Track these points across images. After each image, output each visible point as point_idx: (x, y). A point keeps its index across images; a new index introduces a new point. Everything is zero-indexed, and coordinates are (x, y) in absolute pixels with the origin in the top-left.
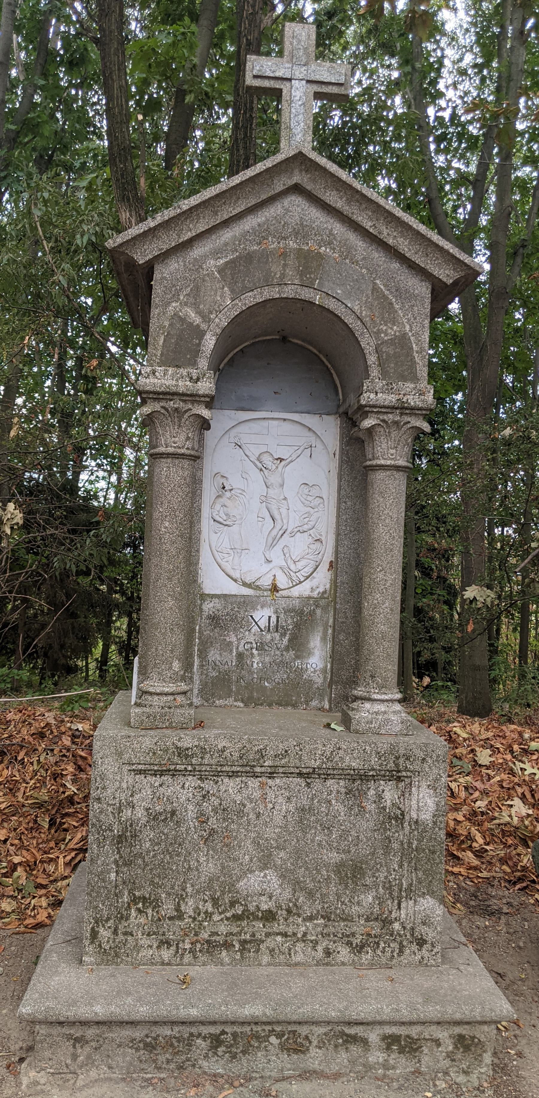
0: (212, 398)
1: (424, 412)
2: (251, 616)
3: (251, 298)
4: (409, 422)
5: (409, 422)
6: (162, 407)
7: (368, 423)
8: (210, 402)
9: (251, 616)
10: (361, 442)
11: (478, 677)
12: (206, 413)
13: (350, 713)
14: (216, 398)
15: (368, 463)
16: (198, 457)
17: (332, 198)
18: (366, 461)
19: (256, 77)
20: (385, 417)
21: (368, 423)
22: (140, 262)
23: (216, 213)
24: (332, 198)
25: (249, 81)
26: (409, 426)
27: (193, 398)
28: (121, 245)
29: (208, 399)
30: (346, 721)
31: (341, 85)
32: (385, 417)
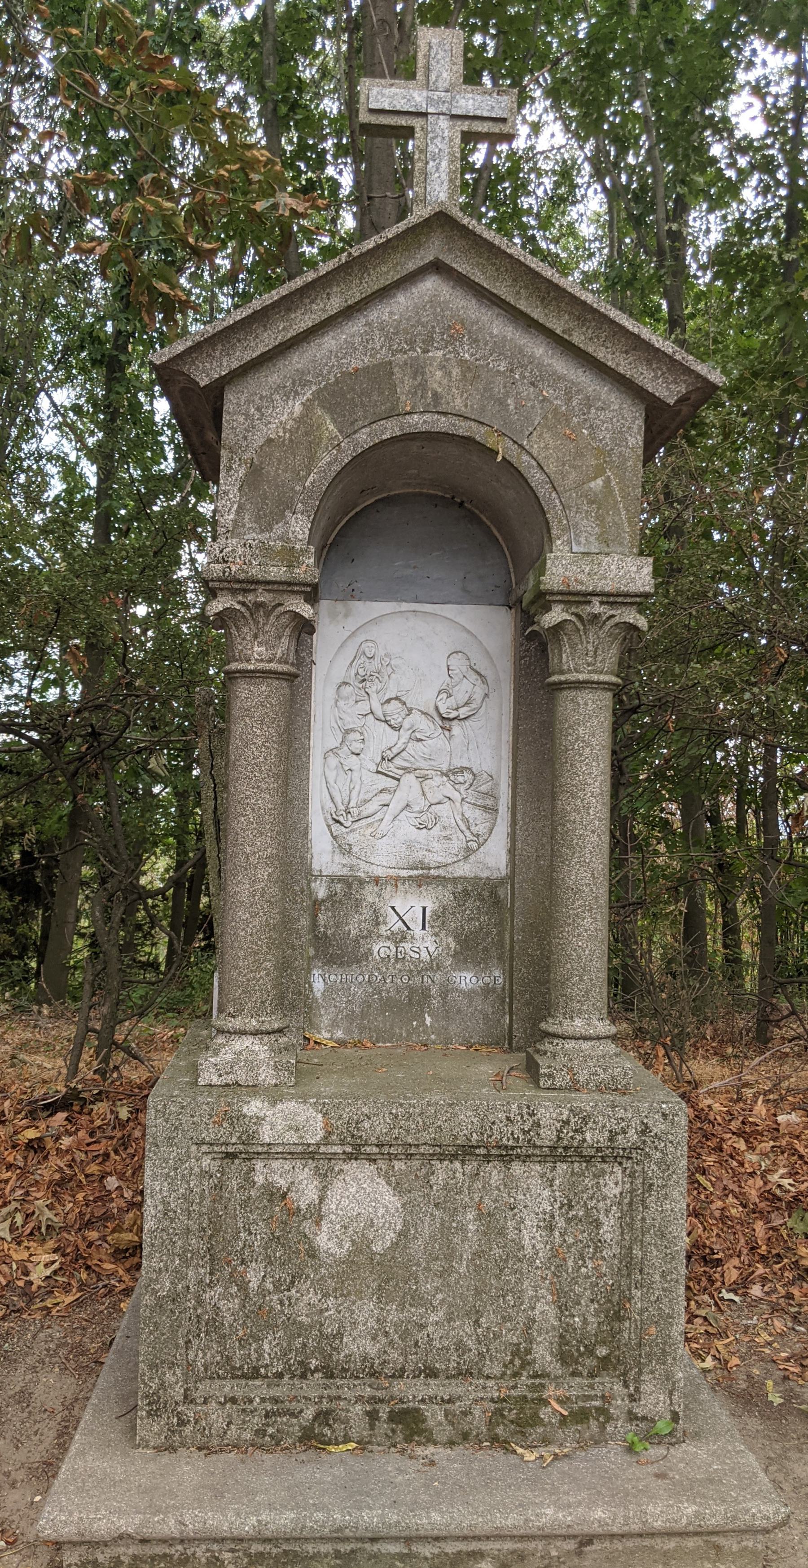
0: (315, 587)
1: (638, 599)
2: (393, 908)
3: (364, 438)
4: (613, 616)
5: (613, 616)
6: (239, 602)
7: (555, 615)
8: (312, 595)
9: (393, 908)
10: (543, 650)
11: (546, 1071)
12: (306, 610)
13: (537, 1057)
14: (321, 586)
15: (555, 678)
16: (296, 676)
17: (303, 321)
18: (550, 676)
19: (372, 111)
20: (578, 610)
21: (555, 615)
22: (202, 384)
23: (496, 279)
24: (303, 321)
25: (364, 117)
26: (612, 622)
27: (288, 587)
28: (171, 360)
29: (309, 589)
30: (532, 1070)
31: (504, 120)
32: (578, 610)
